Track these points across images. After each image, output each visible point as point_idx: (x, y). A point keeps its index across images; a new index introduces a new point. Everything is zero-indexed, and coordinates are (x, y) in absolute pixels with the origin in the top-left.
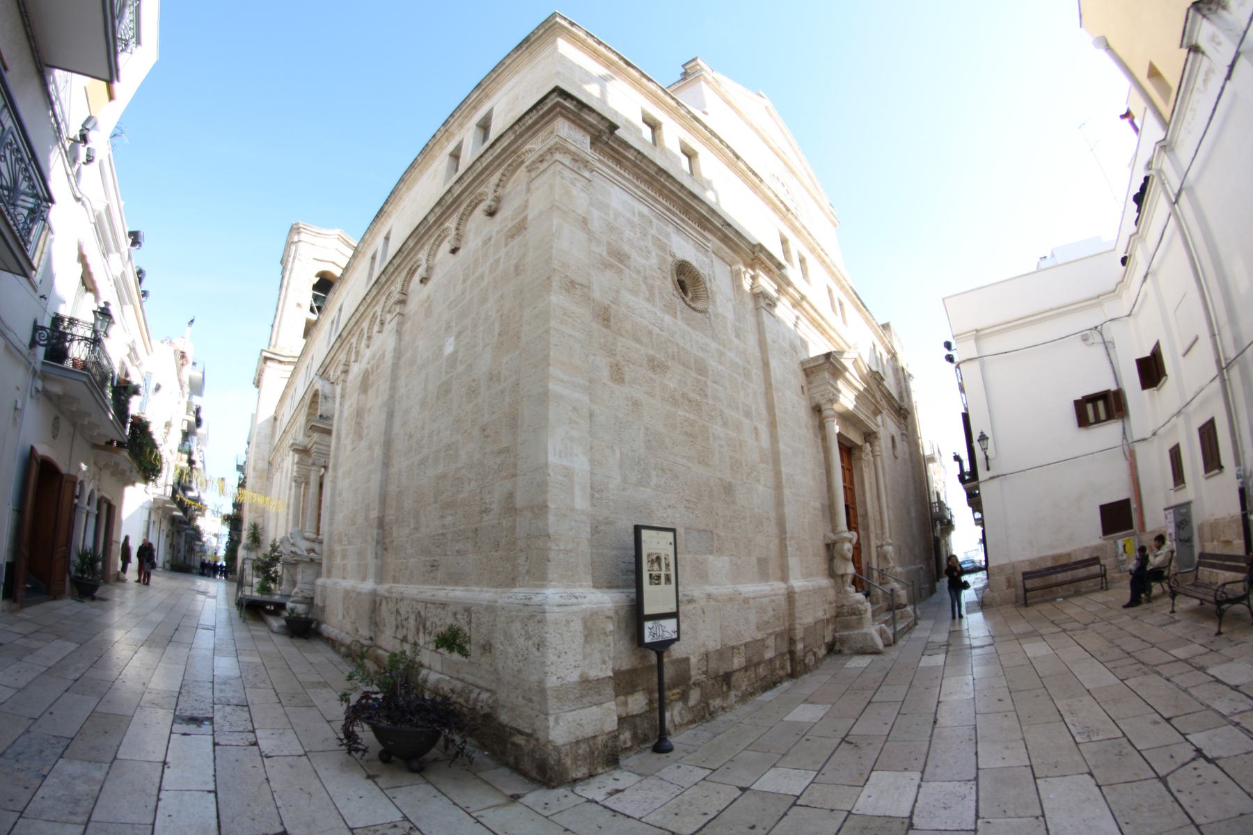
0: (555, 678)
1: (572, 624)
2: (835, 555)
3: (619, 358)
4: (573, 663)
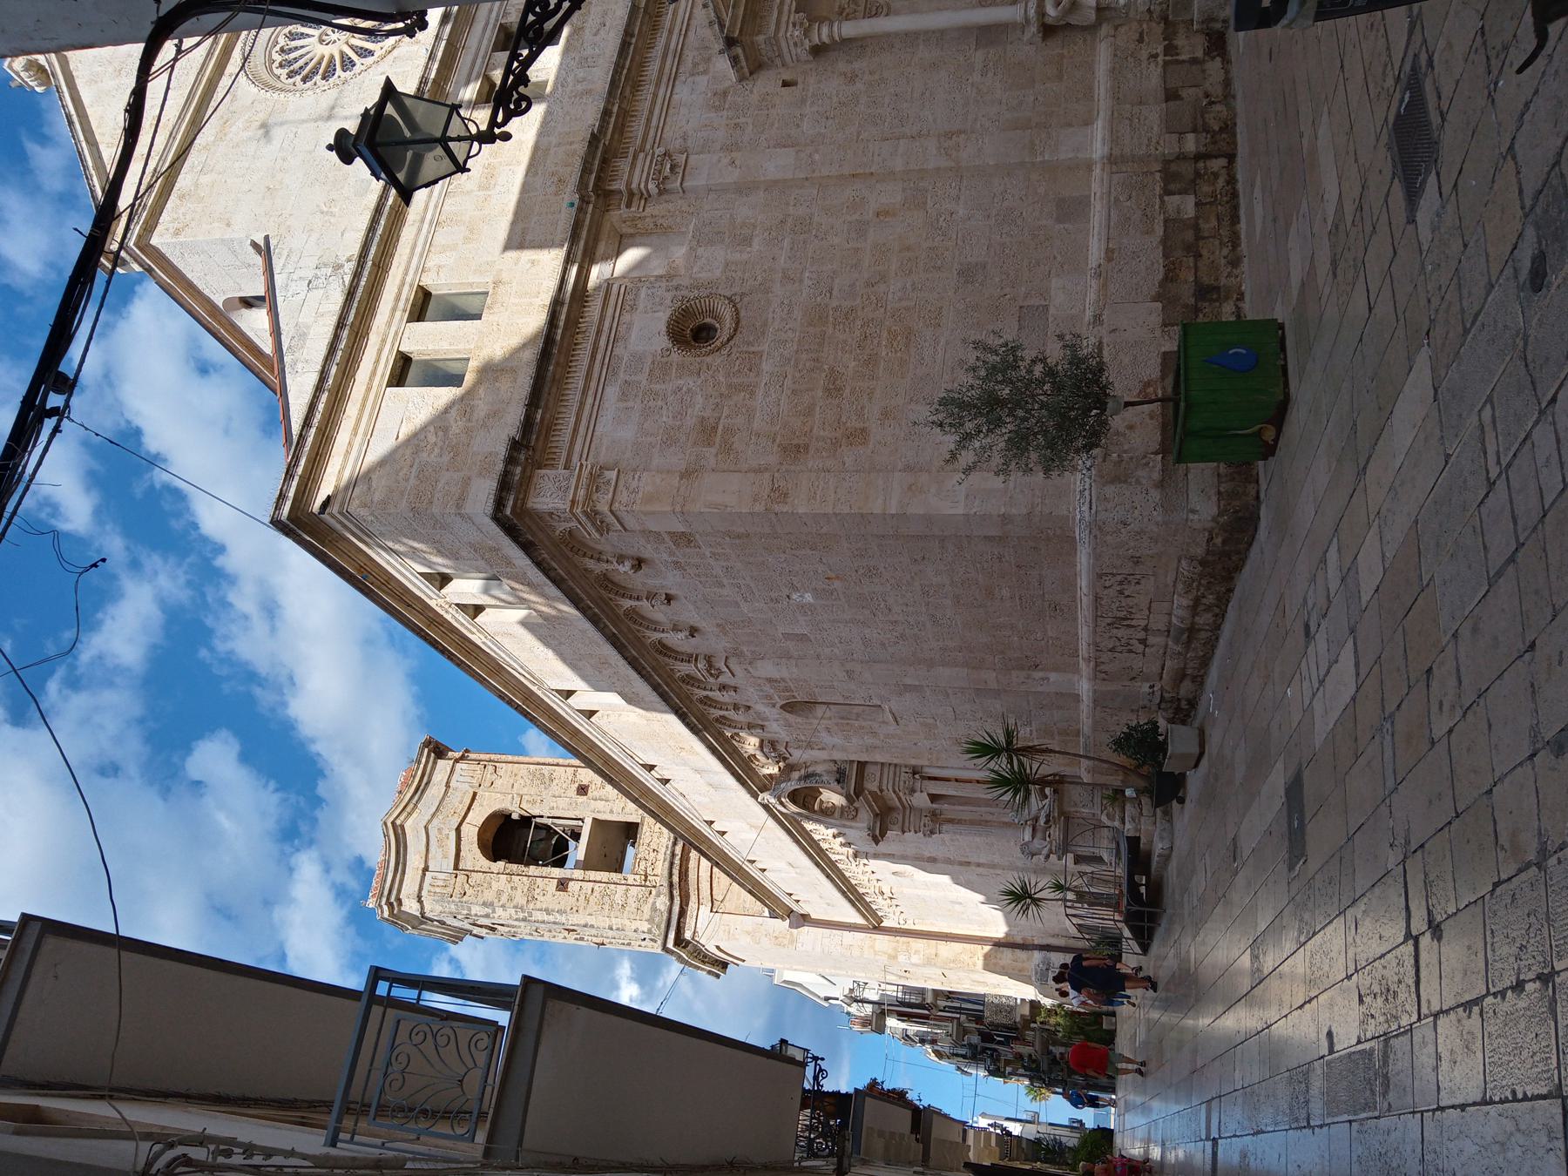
0: (1155, 513)
2: (1062, 23)
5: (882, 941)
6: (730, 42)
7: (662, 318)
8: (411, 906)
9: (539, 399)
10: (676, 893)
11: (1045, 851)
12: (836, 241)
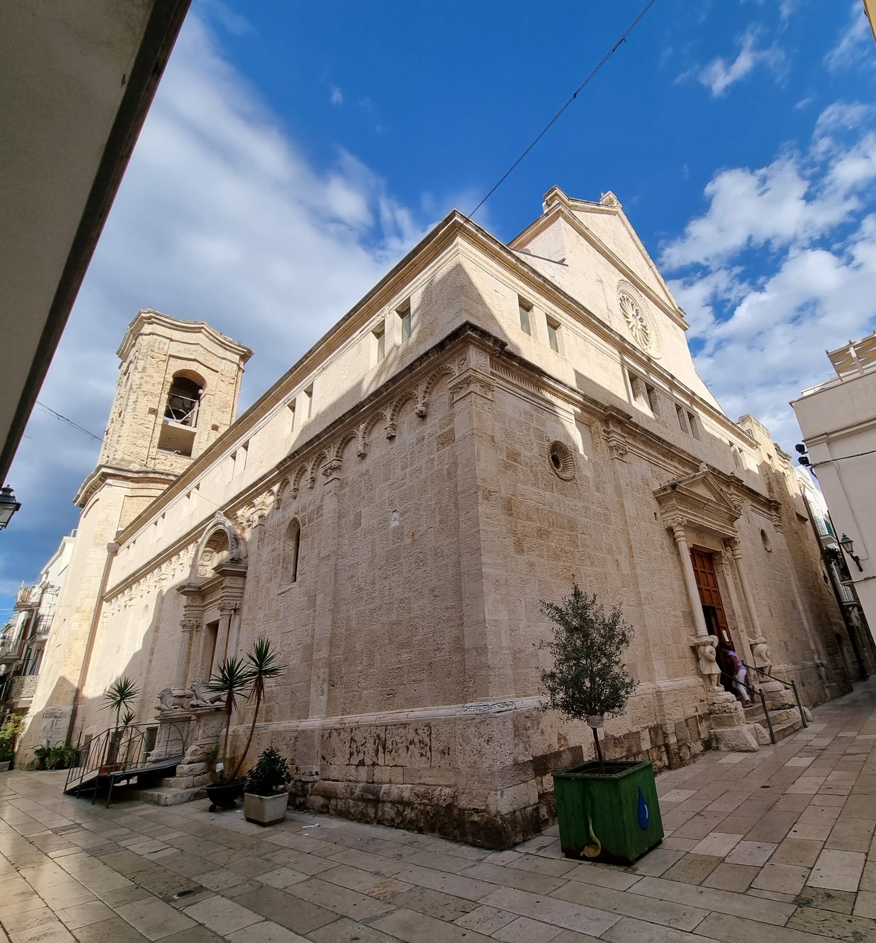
1: (506, 724)
2: (700, 656)
3: (519, 535)
4: (509, 752)
5: (92, 602)
6: (674, 486)
8: (147, 329)
9: (523, 366)
10: (141, 475)
11: (164, 707)
12: (604, 537)
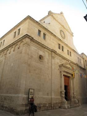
6: (62, 64)
7: (42, 55)
